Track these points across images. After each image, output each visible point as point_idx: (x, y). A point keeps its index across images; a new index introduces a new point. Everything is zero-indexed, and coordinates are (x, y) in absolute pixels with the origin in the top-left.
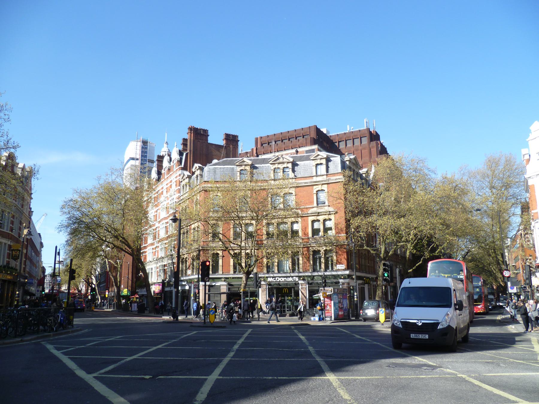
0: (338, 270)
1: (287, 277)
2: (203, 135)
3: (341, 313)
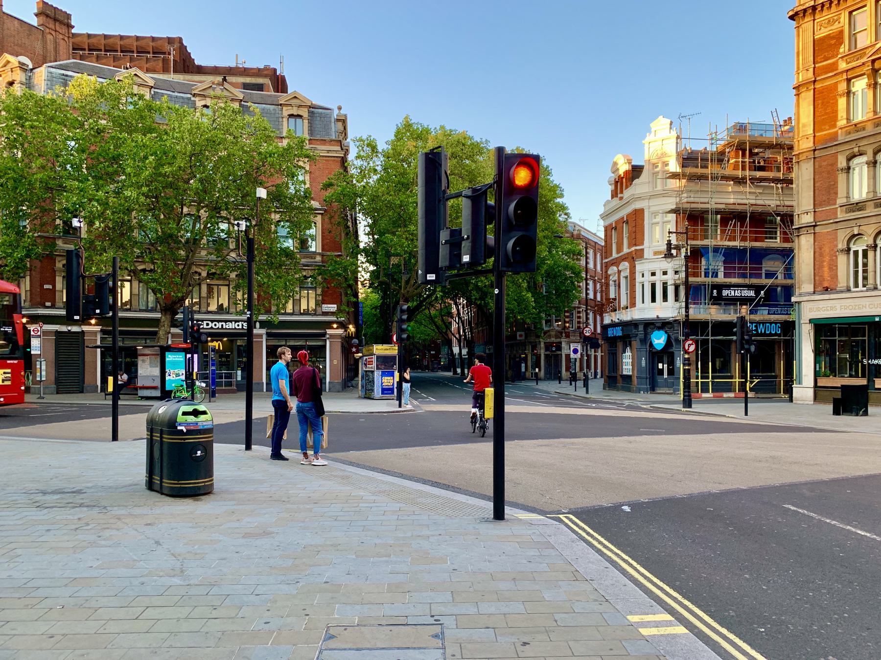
1: (226, 321)
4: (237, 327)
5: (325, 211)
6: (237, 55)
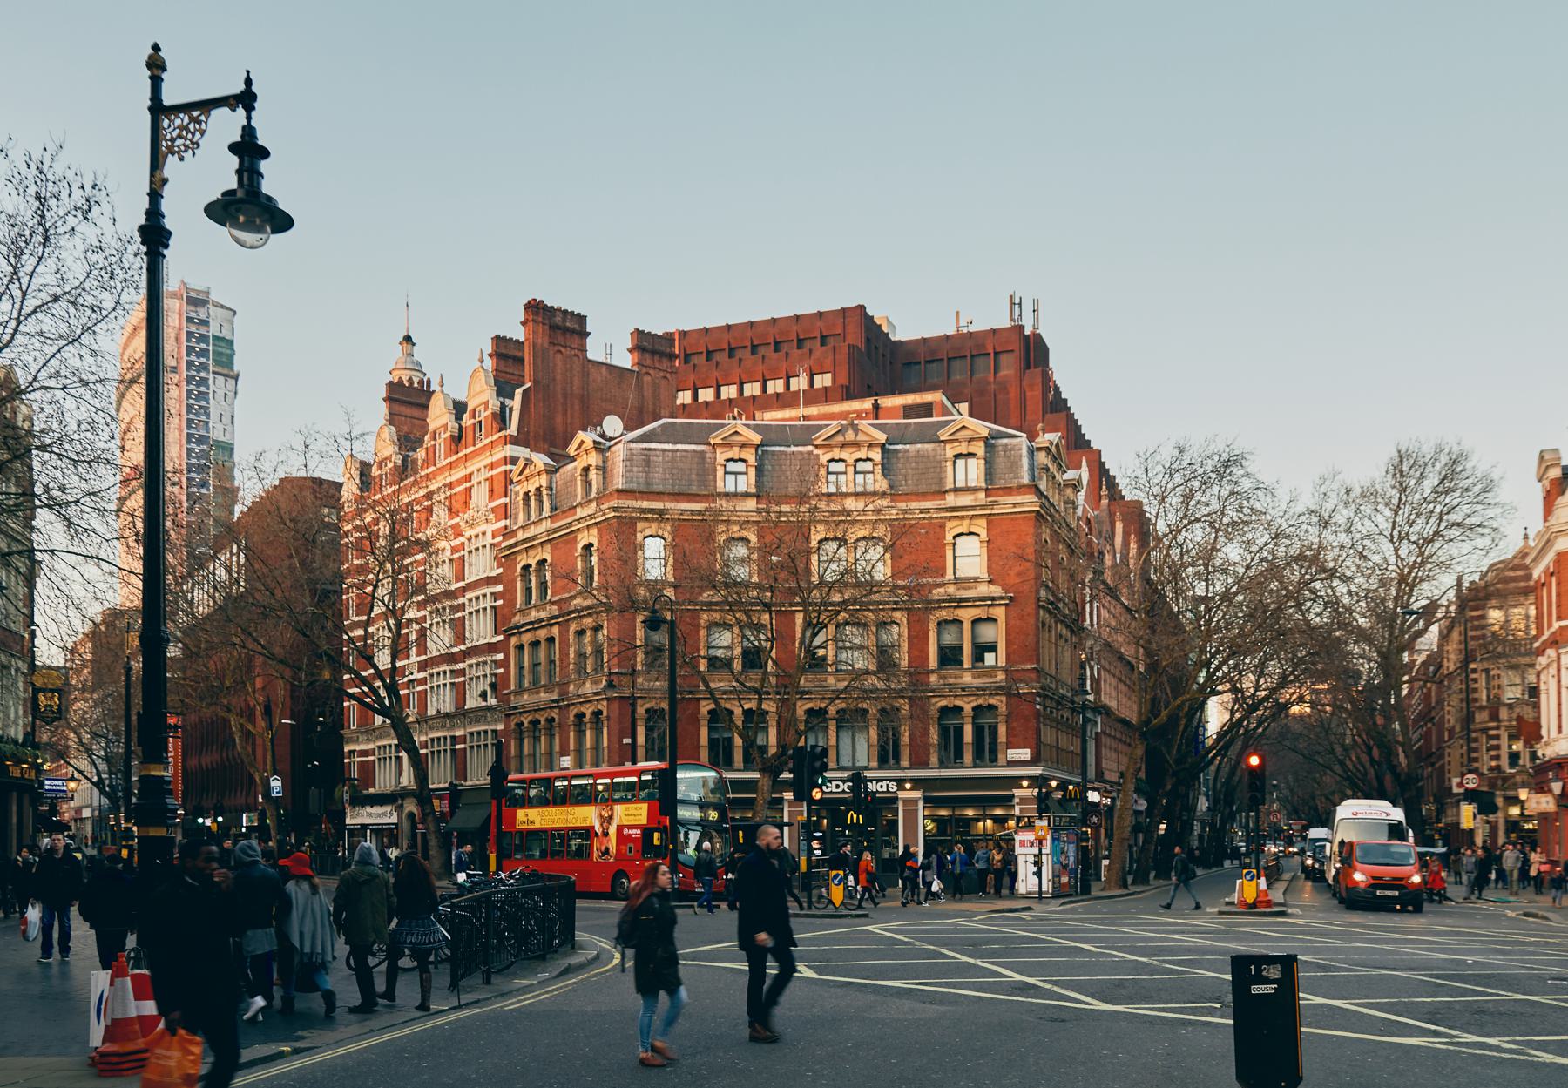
0: (1011, 764)
2: (573, 331)
3: (1065, 879)
4: (880, 790)
5: (1011, 599)
6: (958, 313)
